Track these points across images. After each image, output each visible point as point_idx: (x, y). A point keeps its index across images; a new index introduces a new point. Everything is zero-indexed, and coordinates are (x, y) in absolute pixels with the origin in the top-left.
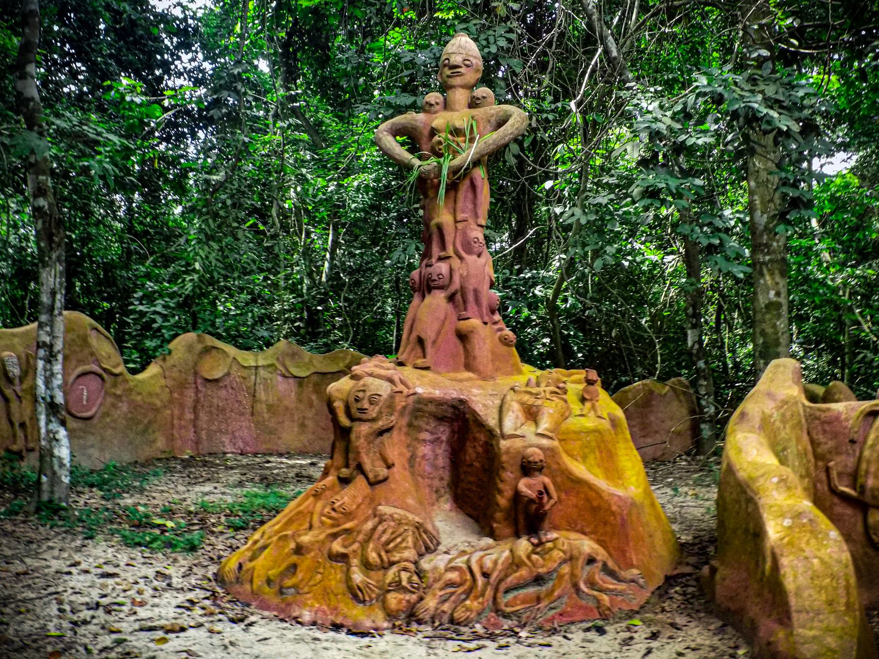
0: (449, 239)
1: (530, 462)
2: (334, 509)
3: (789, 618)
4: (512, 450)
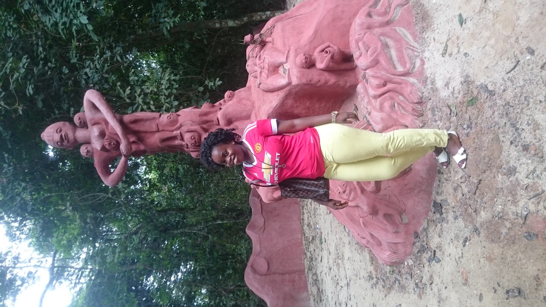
1: (306, 62)
2: (344, 192)
3: (352, 85)
4: (299, 76)
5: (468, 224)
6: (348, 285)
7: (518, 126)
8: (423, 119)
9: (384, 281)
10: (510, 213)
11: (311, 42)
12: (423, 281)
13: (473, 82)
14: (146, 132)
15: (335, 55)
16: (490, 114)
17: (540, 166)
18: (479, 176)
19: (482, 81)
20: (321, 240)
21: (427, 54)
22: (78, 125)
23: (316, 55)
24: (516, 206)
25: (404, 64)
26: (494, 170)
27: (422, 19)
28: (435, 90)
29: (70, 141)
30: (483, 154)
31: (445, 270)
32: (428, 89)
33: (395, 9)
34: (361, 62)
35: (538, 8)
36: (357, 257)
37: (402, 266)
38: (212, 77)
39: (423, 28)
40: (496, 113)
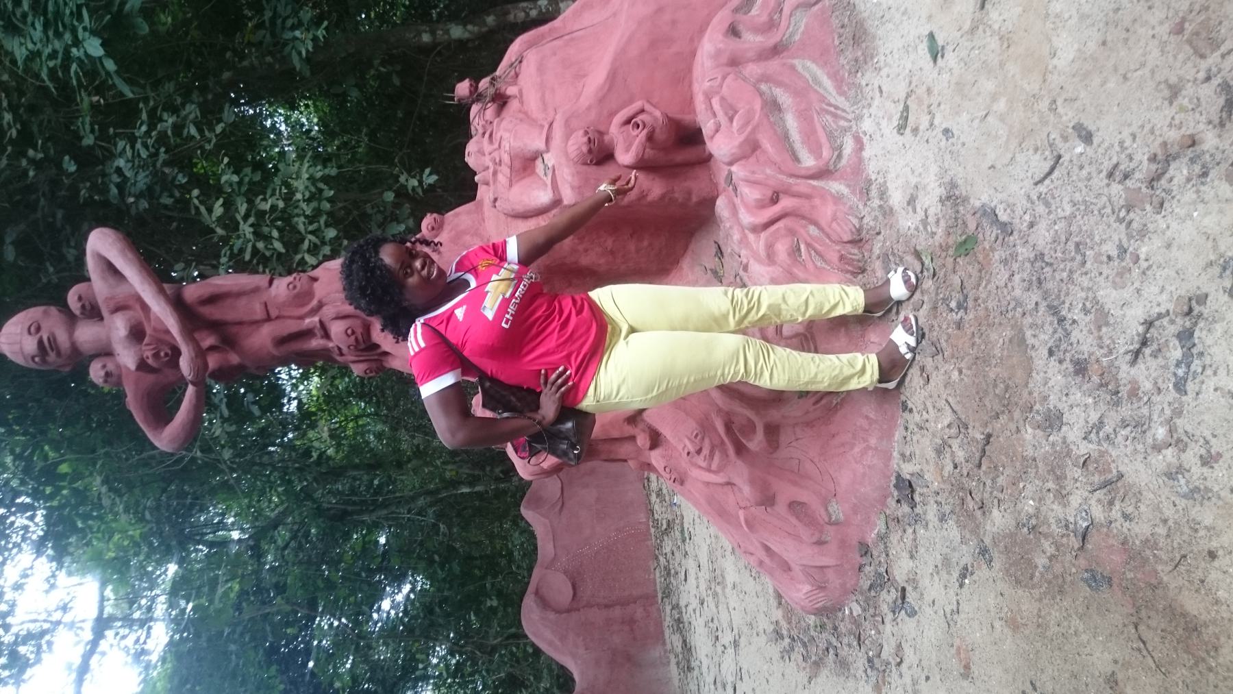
0: (292, 326)
1: (590, 151)
2: (699, 452)
4: (576, 184)
5: (968, 536)
6: (736, 644)
7: (1063, 313)
8: (864, 280)
9: (805, 645)
10: (1052, 521)
11: (601, 100)
12: (884, 655)
13: (966, 200)
14: (241, 323)
15: (658, 131)
16: (1006, 281)
17: (1113, 413)
18: (986, 425)
19: (985, 198)
20: (682, 531)
21: (867, 125)
22: (77, 312)
23: (615, 131)
24: (1065, 506)
25: (816, 150)
26: (1017, 414)
27: (853, 41)
28: (887, 212)
29: (63, 352)
30: (992, 376)
31: (918, 636)
32: (873, 209)
33: (791, 15)
34: (720, 146)
35: (1095, 29)
36: (750, 585)
37: (840, 614)
38: (415, 167)
39: (856, 60)
40: (1017, 278)
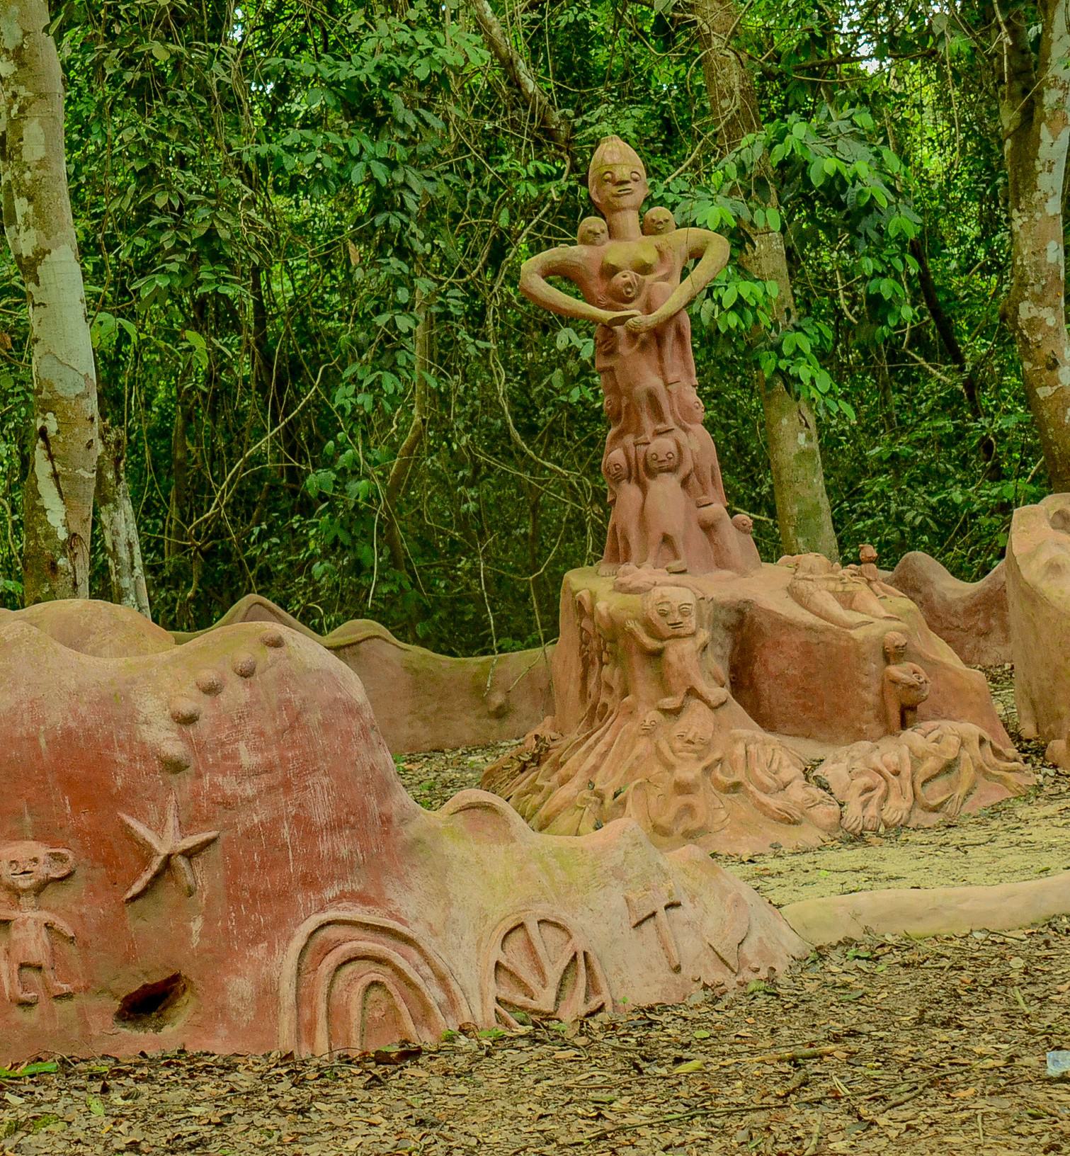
0: (665, 406)
14: (661, 358)
29: (620, 199)
